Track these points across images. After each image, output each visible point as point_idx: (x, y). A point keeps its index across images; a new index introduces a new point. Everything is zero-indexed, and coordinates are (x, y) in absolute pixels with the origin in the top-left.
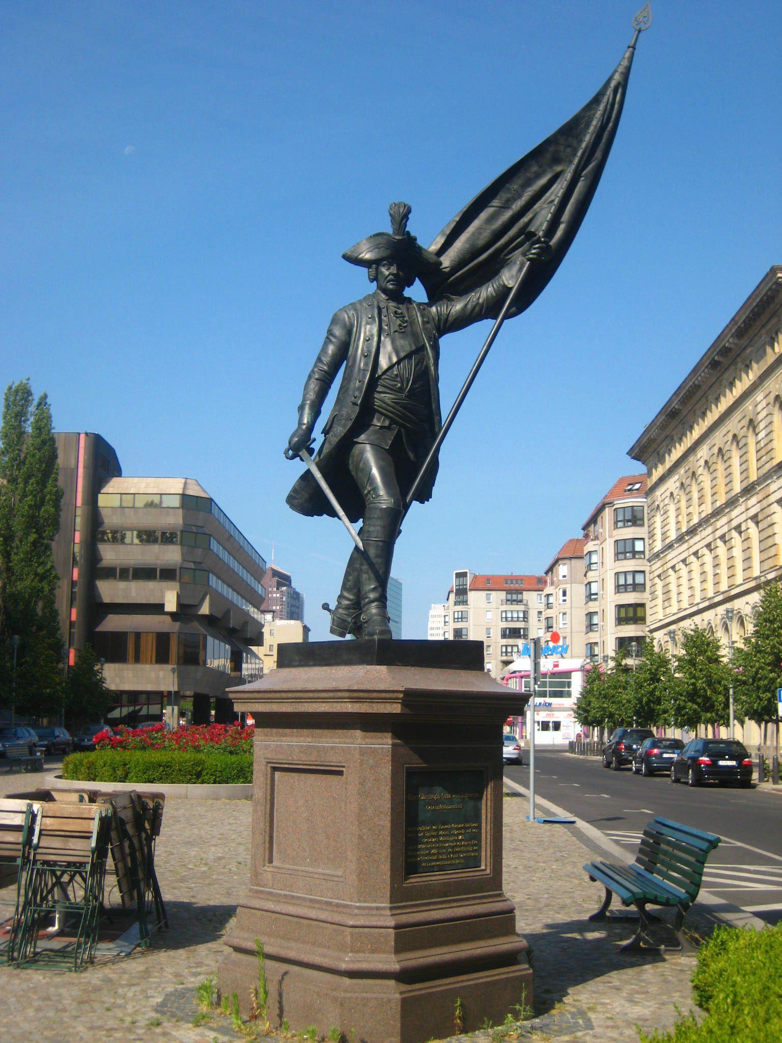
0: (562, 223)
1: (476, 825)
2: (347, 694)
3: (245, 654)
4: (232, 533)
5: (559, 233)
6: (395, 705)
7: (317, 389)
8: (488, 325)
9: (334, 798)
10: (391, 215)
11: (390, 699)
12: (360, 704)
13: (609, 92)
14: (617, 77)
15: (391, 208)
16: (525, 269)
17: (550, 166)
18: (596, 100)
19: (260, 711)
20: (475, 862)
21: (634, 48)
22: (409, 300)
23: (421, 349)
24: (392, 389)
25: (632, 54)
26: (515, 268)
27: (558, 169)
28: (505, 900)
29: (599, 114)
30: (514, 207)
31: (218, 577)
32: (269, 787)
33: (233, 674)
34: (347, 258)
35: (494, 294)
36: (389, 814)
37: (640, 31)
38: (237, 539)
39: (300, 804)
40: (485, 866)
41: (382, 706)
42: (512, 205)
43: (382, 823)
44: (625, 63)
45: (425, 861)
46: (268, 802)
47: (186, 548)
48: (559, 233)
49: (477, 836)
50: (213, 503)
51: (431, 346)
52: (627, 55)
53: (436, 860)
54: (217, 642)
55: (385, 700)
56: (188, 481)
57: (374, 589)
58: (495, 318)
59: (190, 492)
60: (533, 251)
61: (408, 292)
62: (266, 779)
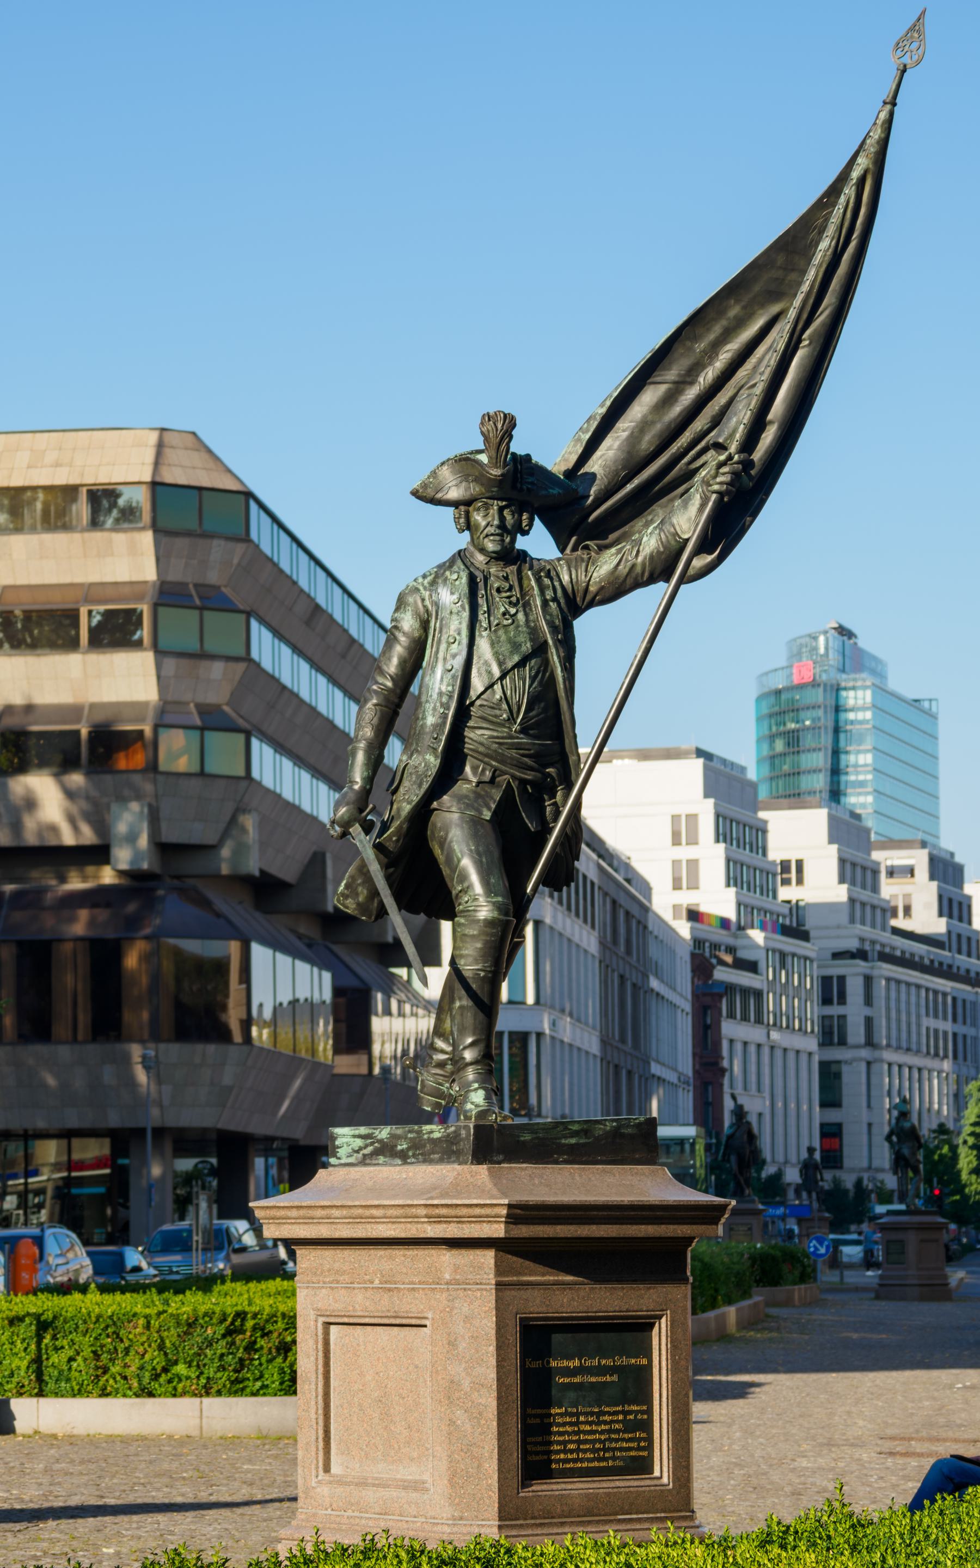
0: (771, 422)
1: (645, 1408)
2: (423, 1212)
3: (379, 996)
4: (321, 600)
5: (768, 437)
6: (496, 1226)
7: (375, 721)
8: (660, 590)
9: (417, 1367)
10: (482, 433)
11: (487, 1216)
12: (445, 1226)
13: (849, 191)
14: (863, 162)
15: (482, 423)
16: (710, 504)
17: (763, 305)
18: (834, 191)
19: (302, 1237)
20: (642, 1466)
21: (894, 104)
22: (523, 556)
23: (540, 649)
24: (494, 723)
25: (891, 114)
26: (696, 501)
27: (775, 309)
28: (698, 1527)
29: (835, 220)
30: (701, 379)
31: (281, 747)
32: (321, 1354)
33: (347, 1064)
34: (415, 493)
35: (662, 549)
36: (495, 1387)
37: (904, 71)
38: (338, 616)
39: (369, 1378)
40: (662, 1470)
41: (477, 1226)
42: (698, 376)
43: (483, 1401)
44: (877, 134)
45: (558, 1461)
46: (321, 1377)
47: (170, 664)
48: (768, 437)
49: (646, 1426)
50: (253, 506)
51: (557, 642)
52: (883, 115)
53: (575, 1461)
54: (284, 960)
55: (479, 1219)
56: (168, 437)
57: (472, 1044)
58: (667, 580)
59: (171, 475)
60: (719, 480)
61: (521, 543)
62: (317, 1342)
